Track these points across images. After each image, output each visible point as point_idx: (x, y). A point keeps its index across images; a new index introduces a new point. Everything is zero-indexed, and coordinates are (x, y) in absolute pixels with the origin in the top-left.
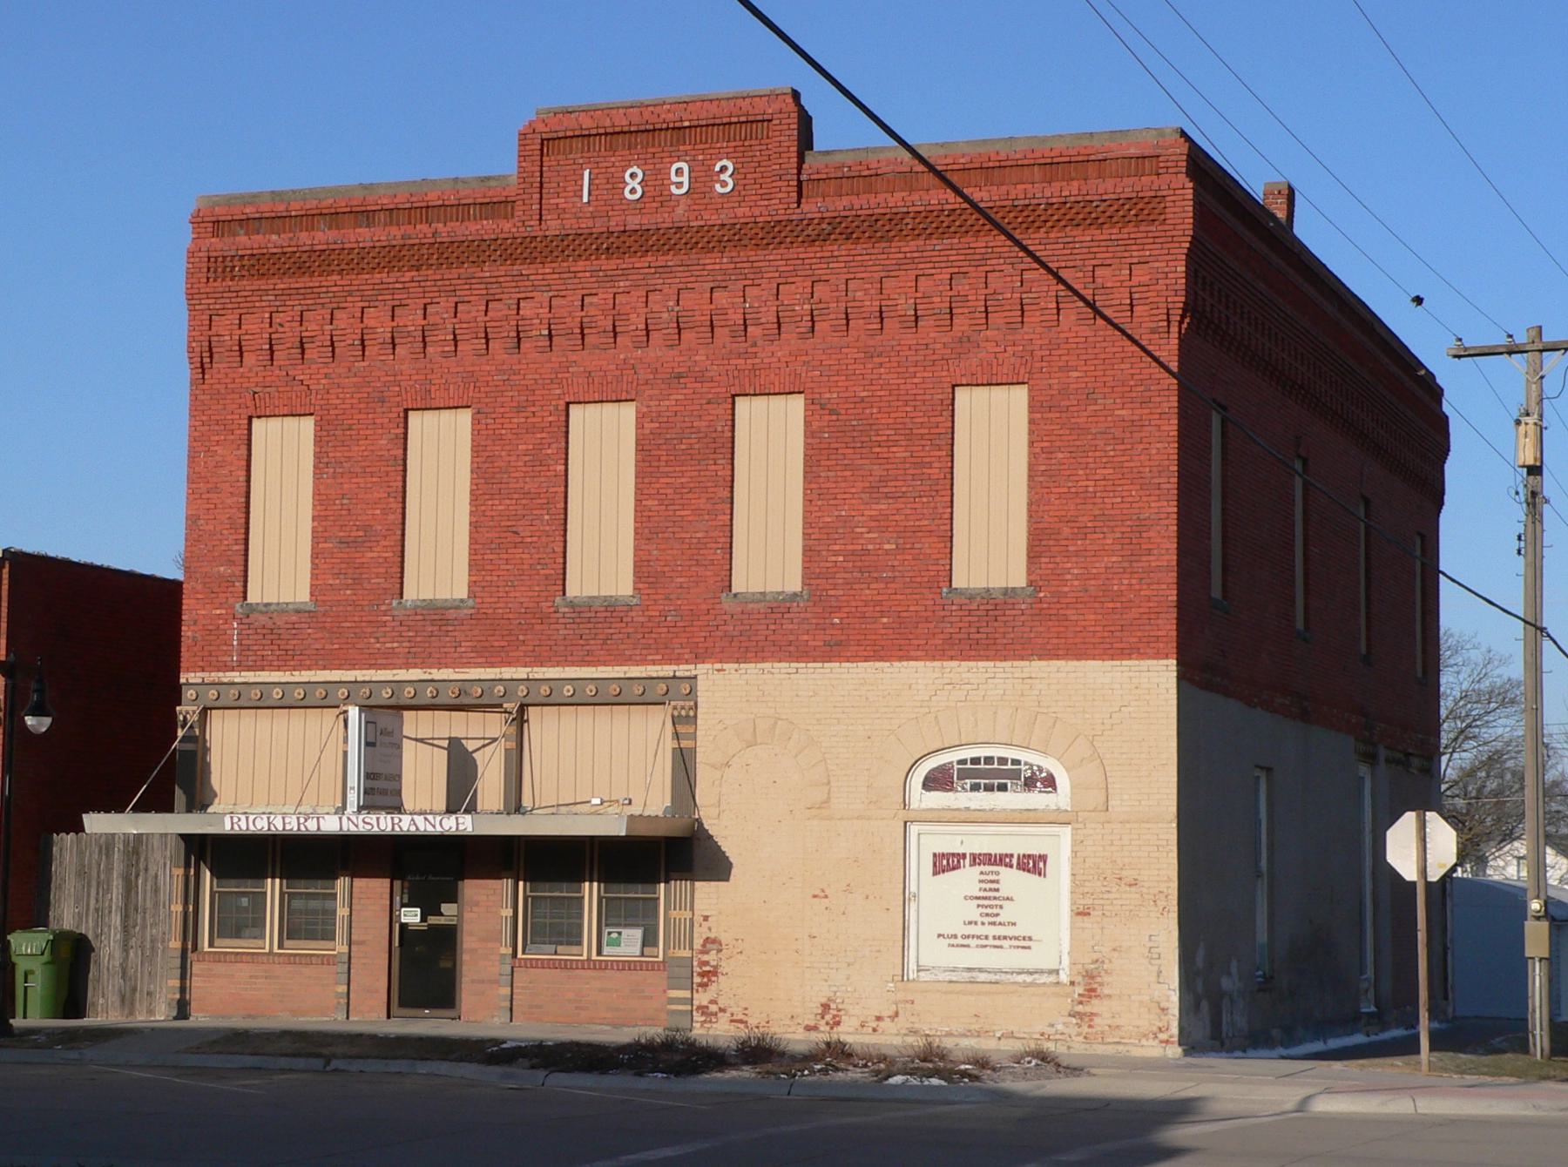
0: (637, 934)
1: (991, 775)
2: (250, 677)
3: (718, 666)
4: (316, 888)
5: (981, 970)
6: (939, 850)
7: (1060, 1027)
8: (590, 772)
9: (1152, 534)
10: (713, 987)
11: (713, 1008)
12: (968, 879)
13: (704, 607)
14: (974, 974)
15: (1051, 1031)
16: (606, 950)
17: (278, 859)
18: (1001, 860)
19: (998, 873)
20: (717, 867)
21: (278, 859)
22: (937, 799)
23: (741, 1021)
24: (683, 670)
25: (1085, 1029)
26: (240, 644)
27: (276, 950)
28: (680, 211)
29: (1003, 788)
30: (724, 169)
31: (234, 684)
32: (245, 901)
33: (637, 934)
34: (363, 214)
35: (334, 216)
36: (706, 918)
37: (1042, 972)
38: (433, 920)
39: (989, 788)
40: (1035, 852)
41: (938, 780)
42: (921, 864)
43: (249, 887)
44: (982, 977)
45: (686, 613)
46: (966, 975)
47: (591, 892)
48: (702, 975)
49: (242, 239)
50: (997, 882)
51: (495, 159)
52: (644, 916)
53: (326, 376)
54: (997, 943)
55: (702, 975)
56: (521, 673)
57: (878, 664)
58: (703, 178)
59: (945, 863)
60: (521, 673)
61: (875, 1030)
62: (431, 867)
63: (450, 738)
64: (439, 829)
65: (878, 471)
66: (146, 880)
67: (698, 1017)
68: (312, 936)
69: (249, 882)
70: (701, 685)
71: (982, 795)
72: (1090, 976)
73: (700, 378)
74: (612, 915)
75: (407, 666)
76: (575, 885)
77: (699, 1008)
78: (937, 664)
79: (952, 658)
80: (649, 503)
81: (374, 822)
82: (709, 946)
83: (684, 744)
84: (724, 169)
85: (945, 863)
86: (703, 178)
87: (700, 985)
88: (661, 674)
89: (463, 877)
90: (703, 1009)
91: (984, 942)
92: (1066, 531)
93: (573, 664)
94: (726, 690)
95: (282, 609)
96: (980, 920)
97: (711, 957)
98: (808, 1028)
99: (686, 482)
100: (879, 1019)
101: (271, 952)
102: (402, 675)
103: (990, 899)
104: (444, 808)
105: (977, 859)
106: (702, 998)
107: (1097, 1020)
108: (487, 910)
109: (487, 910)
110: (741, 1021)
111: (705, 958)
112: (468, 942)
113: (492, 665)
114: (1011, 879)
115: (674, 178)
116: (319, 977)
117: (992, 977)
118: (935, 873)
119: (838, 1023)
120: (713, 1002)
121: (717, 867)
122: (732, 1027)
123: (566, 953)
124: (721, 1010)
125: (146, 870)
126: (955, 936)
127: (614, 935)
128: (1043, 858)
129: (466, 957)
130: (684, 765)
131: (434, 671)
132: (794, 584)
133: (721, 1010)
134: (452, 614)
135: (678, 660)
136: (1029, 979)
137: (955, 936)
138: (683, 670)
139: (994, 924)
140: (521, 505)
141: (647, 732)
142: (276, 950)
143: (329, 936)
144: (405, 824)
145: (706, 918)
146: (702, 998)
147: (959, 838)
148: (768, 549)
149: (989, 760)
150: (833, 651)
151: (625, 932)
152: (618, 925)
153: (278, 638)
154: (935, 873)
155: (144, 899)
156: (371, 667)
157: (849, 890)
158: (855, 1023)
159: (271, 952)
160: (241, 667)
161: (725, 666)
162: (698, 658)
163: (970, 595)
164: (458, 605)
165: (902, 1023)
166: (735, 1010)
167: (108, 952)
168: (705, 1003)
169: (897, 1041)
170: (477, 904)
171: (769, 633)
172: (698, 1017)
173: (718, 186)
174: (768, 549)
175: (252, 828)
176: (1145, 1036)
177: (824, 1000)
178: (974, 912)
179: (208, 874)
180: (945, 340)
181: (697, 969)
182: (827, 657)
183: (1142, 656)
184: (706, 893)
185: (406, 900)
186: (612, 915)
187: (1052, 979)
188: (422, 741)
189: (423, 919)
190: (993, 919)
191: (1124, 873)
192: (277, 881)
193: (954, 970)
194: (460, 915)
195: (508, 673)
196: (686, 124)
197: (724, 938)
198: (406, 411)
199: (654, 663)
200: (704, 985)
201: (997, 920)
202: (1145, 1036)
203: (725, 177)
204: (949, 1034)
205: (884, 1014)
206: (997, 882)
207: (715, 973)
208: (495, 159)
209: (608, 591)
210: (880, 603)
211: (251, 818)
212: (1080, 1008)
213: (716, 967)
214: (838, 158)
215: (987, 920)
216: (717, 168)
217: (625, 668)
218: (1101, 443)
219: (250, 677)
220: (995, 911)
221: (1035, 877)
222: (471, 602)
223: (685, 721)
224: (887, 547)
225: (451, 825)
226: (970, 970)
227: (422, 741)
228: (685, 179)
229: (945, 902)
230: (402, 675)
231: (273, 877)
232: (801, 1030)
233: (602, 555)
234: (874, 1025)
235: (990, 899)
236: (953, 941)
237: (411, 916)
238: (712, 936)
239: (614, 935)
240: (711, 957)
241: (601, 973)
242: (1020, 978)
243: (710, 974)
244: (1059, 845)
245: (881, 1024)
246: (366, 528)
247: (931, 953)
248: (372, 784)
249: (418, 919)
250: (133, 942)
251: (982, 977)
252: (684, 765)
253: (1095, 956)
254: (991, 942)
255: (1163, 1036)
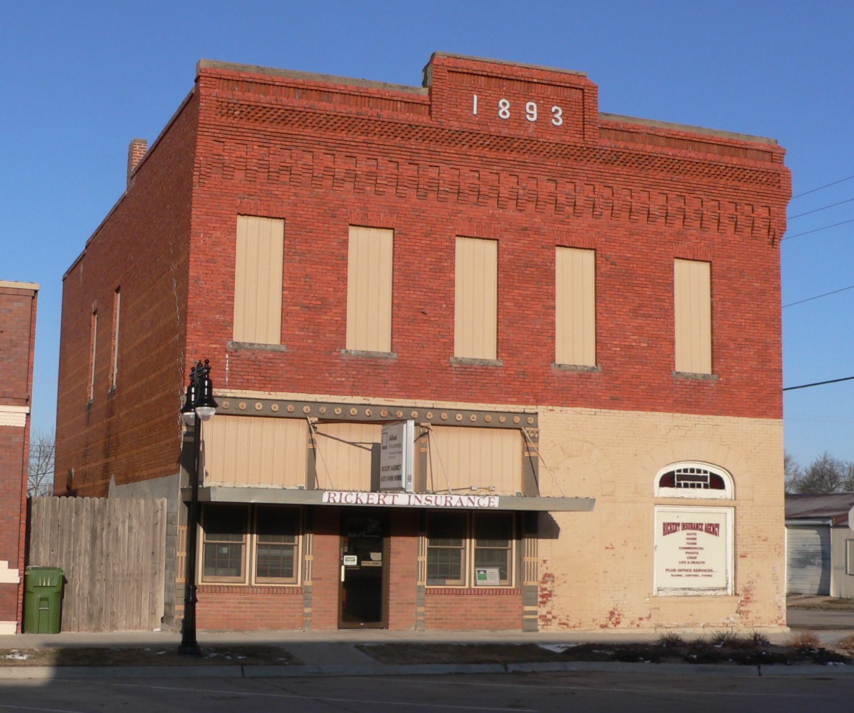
0: (495, 571)
1: (691, 479)
2: (238, 393)
3: (550, 407)
4: (282, 541)
5: (690, 589)
6: (666, 521)
7: (732, 619)
8: (470, 470)
9: (771, 351)
10: (549, 604)
11: (549, 616)
12: (681, 536)
13: (541, 371)
14: (687, 591)
15: (728, 622)
16: (479, 582)
17: (202, 515)
18: (697, 527)
19: (695, 534)
20: (551, 531)
21: (202, 515)
22: (668, 491)
23: (565, 624)
24: (529, 409)
25: (744, 620)
26: (231, 370)
27: (473, 587)
28: (531, 130)
29: (699, 486)
30: (557, 111)
31: (226, 397)
32: (225, 550)
33: (495, 571)
34: (323, 92)
35: (304, 89)
36: (545, 561)
37: (719, 589)
38: (365, 564)
39: (693, 486)
40: (714, 522)
41: (668, 481)
42: (658, 529)
43: (231, 540)
44: (690, 593)
45: (524, 376)
46: (682, 592)
47: (470, 546)
48: (543, 596)
49: (237, 93)
50: (695, 539)
51: (408, 78)
52: (498, 560)
53: (295, 195)
54: (696, 573)
55: (543, 596)
56: (428, 404)
57: (639, 412)
58: (545, 114)
59: (669, 528)
60: (428, 404)
61: (638, 626)
62: (364, 528)
63: (373, 443)
64: (476, 505)
65: (638, 301)
66: (108, 533)
67: (540, 622)
68: (274, 574)
69: (271, 537)
70: (540, 417)
71: (690, 490)
72: (747, 590)
73: (537, 232)
74: (483, 560)
75: (352, 394)
76: (458, 540)
77: (541, 617)
78: (670, 414)
79: (678, 411)
80: (508, 304)
81: (433, 499)
82: (547, 579)
83: (532, 454)
84: (557, 111)
85: (669, 528)
86: (545, 114)
87: (541, 603)
88: (517, 410)
89: (389, 536)
90: (543, 617)
91: (689, 573)
92: (732, 345)
93: (461, 400)
94: (554, 421)
95: (263, 349)
96: (687, 560)
97: (548, 586)
98: (602, 627)
99: (525, 294)
100: (641, 619)
101: (470, 588)
102: (349, 399)
103: (691, 549)
104: (369, 489)
105: (686, 526)
106: (542, 611)
107: (750, 614)
108: (409, 556)
109: (409, 556)
110: (565, 624)
111: (545, 586)
112: (395, 578)
113: (409, 397)
114: (702, 537)
115: (528, 111)
116: (288, 603)
117: (696, 593)
118: (664, 534)
119: (619, 623)
120: (549, 613)
121: (551, 531)
122: (559, 628)
123: (451, 584)
124: (554, 617)
125: (109, 525)
126: (675, 570)
127: (482, 573)
128: (717, 525)
129: (392, 588)
130: (531, 467)
131: (371, 399)
132: (590, 362)
133: (554, 617)
134: (383, 362)
135: (527, 403)
136: (713, 593)
137: (675, 570)
138: (529, 409)
139: (693, 563)
140: (423, 298)
141: (509, 445)
142: (473, 587)
143: (289, 574)
144: (402, 500)
145: (545, 561)
146: (542, 611)
147: (676, 514)
148: (575, 341)
149: (692, 470)
150: (614, 403)
151: (489, 571)
152: (483, 566)
153: (258, 367)
154: (664, 534)
155: (108, 546)
156: (326, 393)
157: (625, 544)
158: (628, 622)
159: (470, 588)
160: (231, 386)
161: (555, 408)
162: (538, 402)
163: (686, 377)
164: (386, 357)
165: (653, 621)
166: (561, 617)
167: (79, 584)
168: (544, 613)
169: (653, 631)
170: (399, 553)
171: (575, 390)
172: (540, 622)
173: (553, 121)
174: (575, 341)
175: (343, 501)
176: (772, 622)
177: (611, 610)
178: (683, 555)
179: (202, 530)
180: (670, 231)
181: (540, 593)
182: (611, 407)
183: (768, 416)
184: (544, 546)
185: (346, 550)
186: (483, 560)
187: (724, 593)
188: (353, 444)
189: (359, 563)
190: (693, 559)
191: (761, 534)
192: (473, 540)
193: (676, 589)
194: (386, 559)
195: (421, 403)
196: (535, 81)
197: (556, 574)
198: (393, 229)
199: (512, 403)
200: (544, 603)
201: (695, 560)
202: (772, 622)
203: (557, 116)
204: (678, 626)
205: (644, 616)
206: (695, 539)
207: (550, 595)
208: (408, 78)
209: (579, 362)
210: (638, 377)
211: (344, 494)
212: (742, 609)
213: (551, 592)
214: (613, 119)
215: (690, 560)
216: (553, 110)
217: (494, 405)
218: (747, 299)
219: (238, 393)
220: (694, 555)
221: (714, 536)
222: (395, 355)
223: (529, 442)
224: (643, 345)
225: (374, 499)
226: (684, 589)
227: (353, 444)
228: (535, 112)
229: (668, 551)
230: (349, 399)
231: (252, 533)
232: (598, 628)
233: (475, 333)
234: (638, 622)
235: (691, 549)
236: (674, 573)
237: (351, 561)
238: (549, 572)
239: (482, 573)
240: (548, 586)
241: (480, 597)
242: (709, 593)
243: (548, 596)
244: (725, 519)
245: (642, 622)
246: (321, 299)
247: (661, 579)
248: (396, 473)
249: (355, 563)
250: (98, 577)
251: (690, 593)
252: (531, 467)
253: (749, 580)
254: (693, 573)
255: (780, 622)
